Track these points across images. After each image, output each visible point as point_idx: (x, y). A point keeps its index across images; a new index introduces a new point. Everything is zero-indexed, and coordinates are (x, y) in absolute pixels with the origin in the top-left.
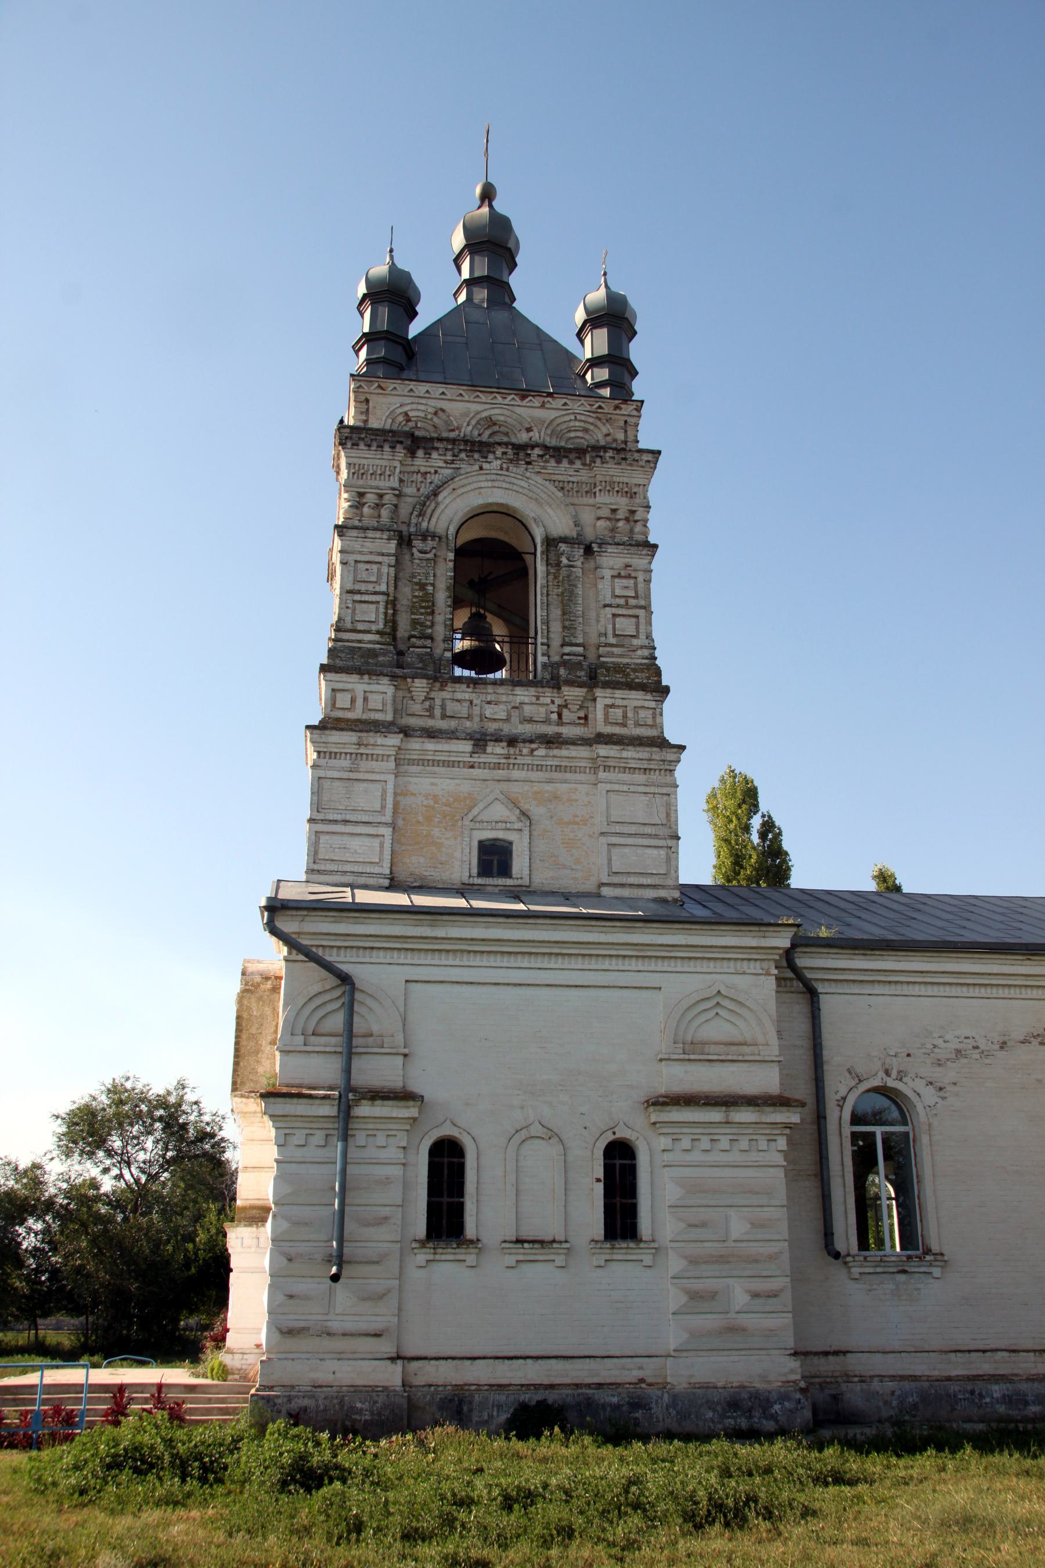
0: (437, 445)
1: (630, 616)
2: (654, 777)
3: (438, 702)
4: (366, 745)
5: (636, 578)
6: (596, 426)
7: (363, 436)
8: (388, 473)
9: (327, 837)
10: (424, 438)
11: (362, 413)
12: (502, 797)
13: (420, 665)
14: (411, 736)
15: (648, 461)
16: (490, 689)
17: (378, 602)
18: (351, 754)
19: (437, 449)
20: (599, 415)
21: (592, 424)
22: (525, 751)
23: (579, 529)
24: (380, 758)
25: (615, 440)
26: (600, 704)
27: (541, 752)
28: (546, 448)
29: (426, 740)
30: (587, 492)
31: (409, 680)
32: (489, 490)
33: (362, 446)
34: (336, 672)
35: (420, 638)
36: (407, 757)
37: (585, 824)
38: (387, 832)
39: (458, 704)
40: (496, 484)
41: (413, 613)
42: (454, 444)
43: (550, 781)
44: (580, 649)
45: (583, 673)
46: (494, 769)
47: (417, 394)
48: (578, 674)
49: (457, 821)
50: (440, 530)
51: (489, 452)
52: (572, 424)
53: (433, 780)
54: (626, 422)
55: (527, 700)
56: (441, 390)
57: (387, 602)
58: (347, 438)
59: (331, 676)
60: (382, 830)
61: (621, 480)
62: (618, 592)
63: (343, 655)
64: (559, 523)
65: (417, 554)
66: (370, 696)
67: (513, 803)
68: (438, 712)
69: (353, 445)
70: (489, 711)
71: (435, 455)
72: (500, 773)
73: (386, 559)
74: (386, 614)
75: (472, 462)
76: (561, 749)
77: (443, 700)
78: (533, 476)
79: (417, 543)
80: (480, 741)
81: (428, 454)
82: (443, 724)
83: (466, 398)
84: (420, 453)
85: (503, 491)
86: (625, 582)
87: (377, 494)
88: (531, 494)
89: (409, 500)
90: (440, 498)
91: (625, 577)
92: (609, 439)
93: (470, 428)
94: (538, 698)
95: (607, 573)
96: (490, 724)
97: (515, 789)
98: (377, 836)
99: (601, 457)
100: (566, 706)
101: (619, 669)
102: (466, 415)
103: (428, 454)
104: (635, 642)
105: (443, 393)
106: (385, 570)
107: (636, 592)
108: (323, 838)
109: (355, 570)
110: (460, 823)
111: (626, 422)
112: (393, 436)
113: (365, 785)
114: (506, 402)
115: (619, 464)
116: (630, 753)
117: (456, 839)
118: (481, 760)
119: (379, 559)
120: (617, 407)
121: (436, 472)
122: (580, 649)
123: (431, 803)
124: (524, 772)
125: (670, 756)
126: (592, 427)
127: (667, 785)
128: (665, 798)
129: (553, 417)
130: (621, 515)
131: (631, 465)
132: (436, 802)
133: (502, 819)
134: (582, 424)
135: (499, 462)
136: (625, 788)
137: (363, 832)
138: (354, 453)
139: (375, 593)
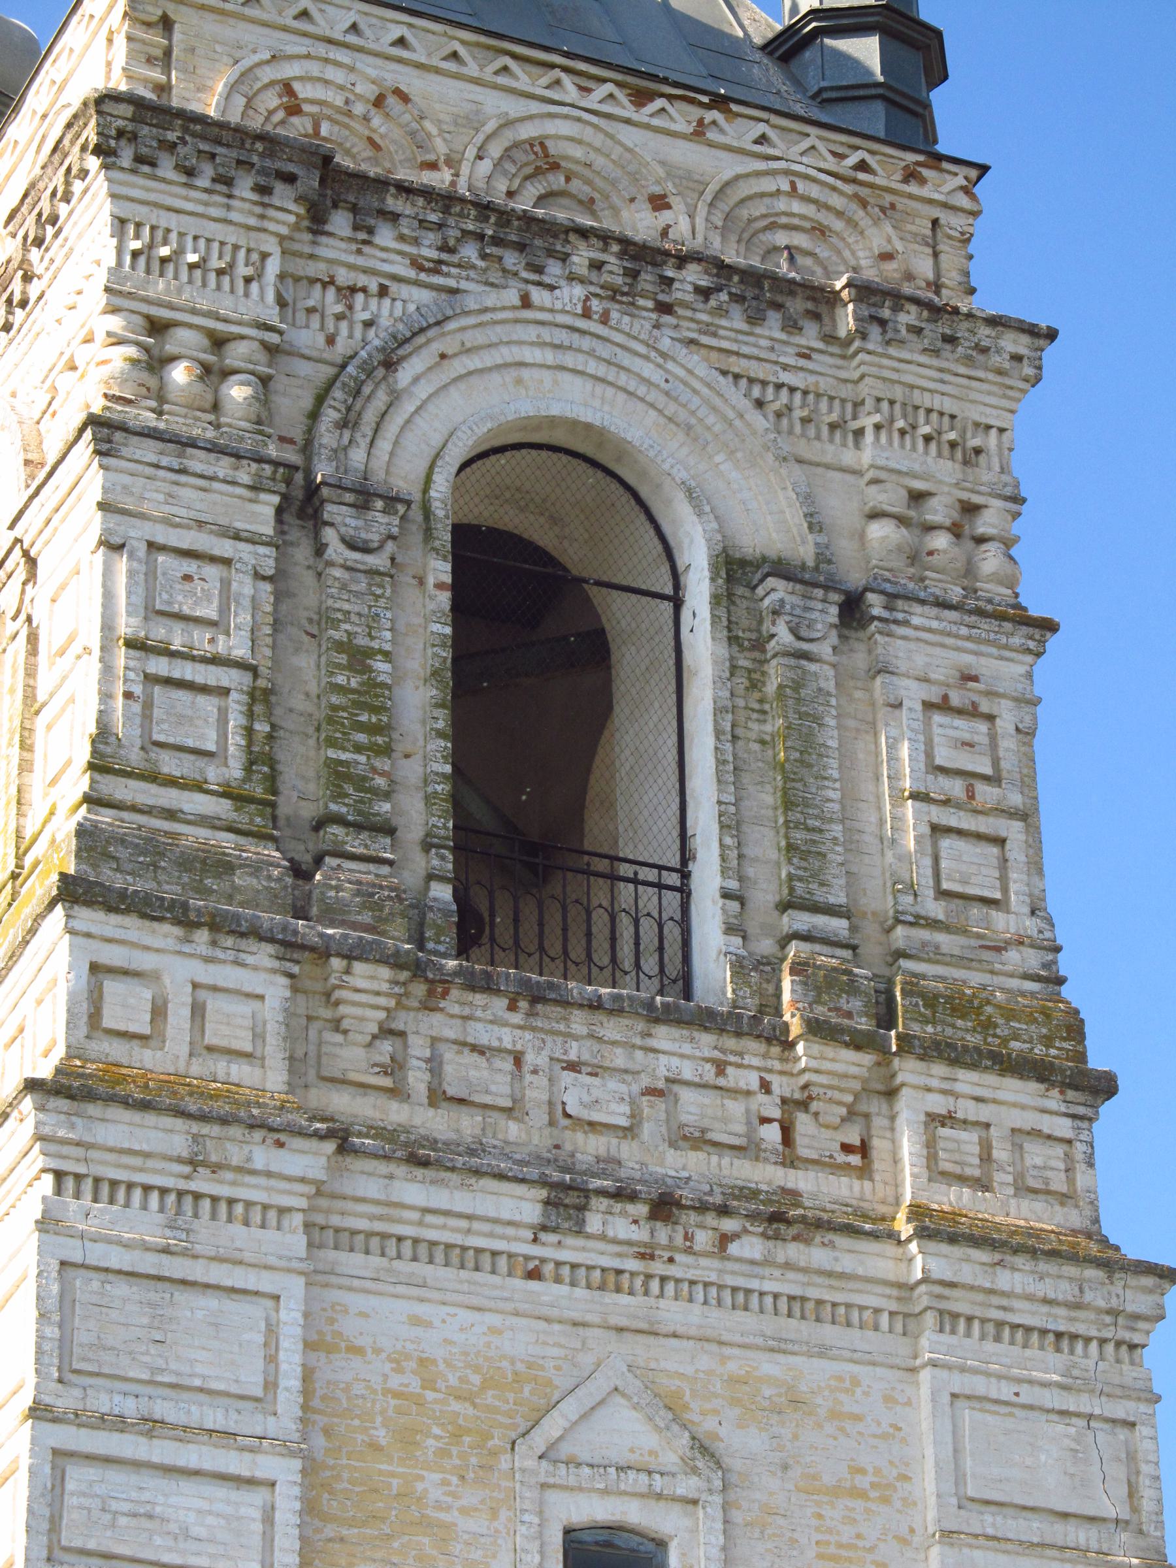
0: (393, 203)
1: (979, 837)
2: (1087, 1359)
3: (418, 1048)
4: (215, 1168)
5: (990, 718)
6: (852, 223)
7: (172, 136)
8: (242, 270)
9: (91, 1472)
10: (361, 178)
11: (150, 60)
12: (633, 1385)
13: (366, 918)
14: (356, 1152)
15: (1017, 358)
16: (579, 1022)
17: (225, 692)
18: (164, 1191)
19: (394, 217)
20: (864, 192)
21: (839, 214)
22: (703, 1239)
23: (822, 539)
24: (439, 1256)
25: (909, 277)
26: (909, 1111)
27: (750, 1247)
28: (722, 268)
29: (401, 1170)
30: (833, 427)
31: (336, 963)
32: (547, 375)
33: (166, 168)
34: (111, 909)
35: (359, 827)
36: (336, 1220)
37: (886, 1500)
38: (285, 1471)
39: (481, 1061)
40: (569, 360)
41: (331, 743)
42: (446, 210)
43: (778, 1347)
44: (838, 926)
45: (856, 1004)
46: (602, 1287)
47: (322, 26)
48: (843, 1003)
49: (494, 1453)
50: (405, 477)
51: (551, 253)
52: (782, 205)
53: (421, 1309)
54: (935, 223)
55: (688, 1071)
56: (396, 32)
57: (253, 694)
58: (121, 133)
59: (89, 918)
60: (267, 1466)
61: (937, 402)
62: (942, 757)
63: (123, 853)
64: (769, 520)
65: (336, 549)
66: (215, 1004)
67: (671, 1409)
68: (417, 1079)
69: (139, 159)
70: (576, 1094)
71: (385, 236)
72: (623, 1306)
73: (244, 552)
74: (249, 731)
75: (495, 276)
76: (808, 1242)
77: (434, 1041)
78: (682, 352)
79: (340, 515)
80: (568, 1199)
81: (364, 229)
82: (437, 1123)
83: (472, 69)
84: (340, 222)
85: (589, 385)
86: (963, 727)
87: (211, 334)
88: (671, 409)
89: (304, 368)
90: (403, 376)
91: (960, 712)
92: (890, 267)
93: (485, 167)
94: (720, 1068)
95: (913, 693)
96: (580, 1136)
97: (674, 1361)
98: (251, 1482)
99: (882, 323)
100: (804, 1105)
101: (961, 1005)
102: (473, 121)
103: (364, 229)
104: (999, 919)
105: (401, 42)
106: (244, 586)
107: (996, 763)
108: (78, 1477)
109: (151, 574)
110: (504, 1462)
111: (935, 223)
112: (269, 154)
113: (212, 1302)
114: (592, 102)
115: (936, 352)
116: (1017, 1278)
117: (494, 1513)
118: (565, 1255)
119: (225, 547)
120: (910, 175)
121: (383, 291)
122: (838, 926)
123: (415, 1385)
124: (697, 1308)
125: (1134, 1296)
126: (838, 225)
127: (1126, 1392)
128: (1122, 1434)
129: (727, 175)
130: (939, 511)
131: (968, 360)
132: (429, 1384)
133: (633, 1458)
134: (809, 210)
135: (579, 291)
136: (1005, 1391)
137: (207, 1466)
138: (139, 187)
139: (214, 660)
